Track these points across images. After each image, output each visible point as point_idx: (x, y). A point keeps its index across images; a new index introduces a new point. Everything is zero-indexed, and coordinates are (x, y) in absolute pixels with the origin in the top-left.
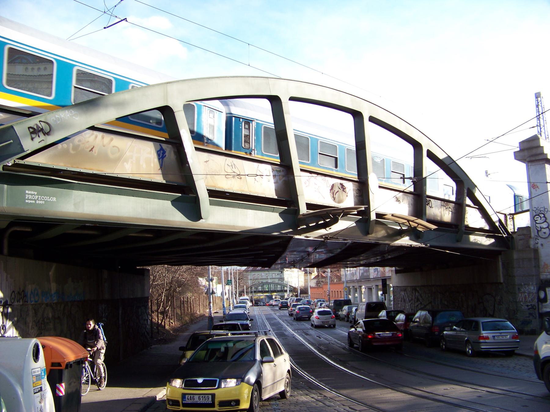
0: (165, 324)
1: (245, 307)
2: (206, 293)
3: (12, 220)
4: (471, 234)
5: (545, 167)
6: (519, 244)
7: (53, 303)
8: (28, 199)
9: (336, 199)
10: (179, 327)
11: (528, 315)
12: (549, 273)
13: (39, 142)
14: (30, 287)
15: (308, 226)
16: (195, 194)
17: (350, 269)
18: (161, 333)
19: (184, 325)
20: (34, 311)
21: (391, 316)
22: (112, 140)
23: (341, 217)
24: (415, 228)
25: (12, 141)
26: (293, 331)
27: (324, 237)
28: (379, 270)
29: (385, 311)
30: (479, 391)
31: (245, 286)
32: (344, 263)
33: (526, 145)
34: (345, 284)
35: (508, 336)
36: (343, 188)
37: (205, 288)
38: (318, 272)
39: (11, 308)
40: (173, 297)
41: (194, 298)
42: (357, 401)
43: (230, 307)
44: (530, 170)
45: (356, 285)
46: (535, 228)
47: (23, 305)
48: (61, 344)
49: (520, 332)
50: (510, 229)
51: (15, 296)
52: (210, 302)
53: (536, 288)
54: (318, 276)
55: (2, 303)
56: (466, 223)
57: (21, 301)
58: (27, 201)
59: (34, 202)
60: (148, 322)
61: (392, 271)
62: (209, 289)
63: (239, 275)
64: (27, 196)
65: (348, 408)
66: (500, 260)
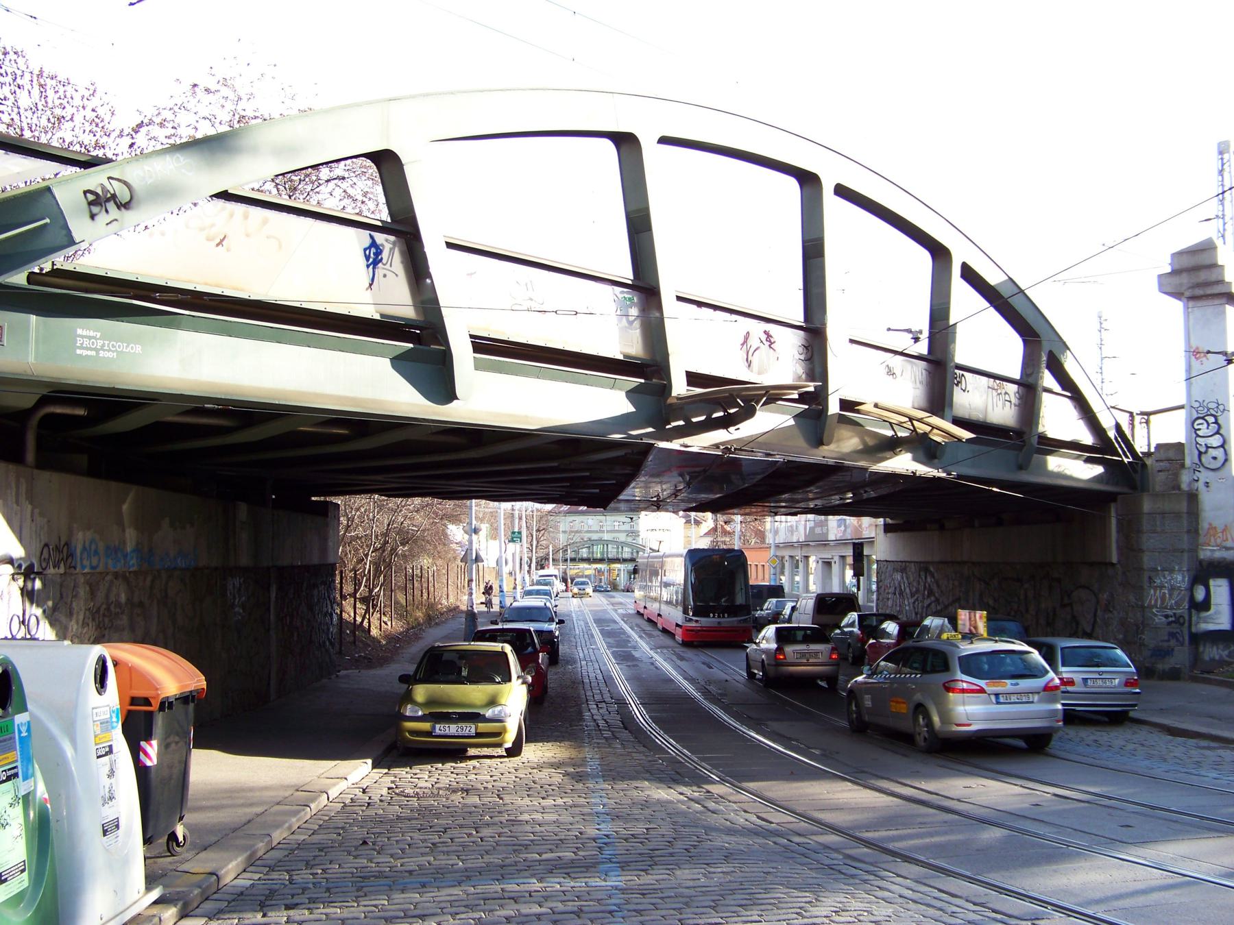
0: (369, 626)
1: (547, 593)
2: (464, 559)
3: (45, 392)
4: (1050, 453)
5: (1224, 312)
6: (1159, 481)
7: (130, 572)
8: (82, 348)
9: (754, 364)
10: (401, 633)
11: (1166, 638)
12: (1218, 546)
13: (107, 224)
14: (80, 535)
15: (688, 421)
16: (441, 345)
17: (786, 519)
18: (361, 645)
19: (413, 628)
20: (88, 588)
21: (870, 626)
22: (265, 222)
23: (763, 405)
24: (925, 434)
25: (48, 220)
26: (651, 649)
27: (722, 447)
28: (848, 522)
29: (855, 614)
30: (1038, 792)
31: (551, 546)
32: (772, 505)
33: (1187, 262)
34: (772, 551)
35: (1117, 681)
36: (770, 341)
37: (461, 547)
38: (716, 521)
39: (41, 579)
40: (389, 566)
41: (435, 568)
42: (777, 806)
43: (515, 593)
44: (1191, 317)
45: (798, 554)
46: (1194, 445)
47: (65, 573)
48: (141, 656)
49: (1146, 672)
50: (1140, 446)
51: (50, 554)
52: (472, 580)
53: (1187, 579)
54: (715, 529)
55: (23, 568)
56: (1041, 429)
57: (62, 565)
58: (79, 352)
59: (93, 353)
60: (332, 619)
61: (876, 526)
62: (468, 551)
63: (539, 521)
64: (79, 342)
65: (754, 818)
66: (1113, 514)
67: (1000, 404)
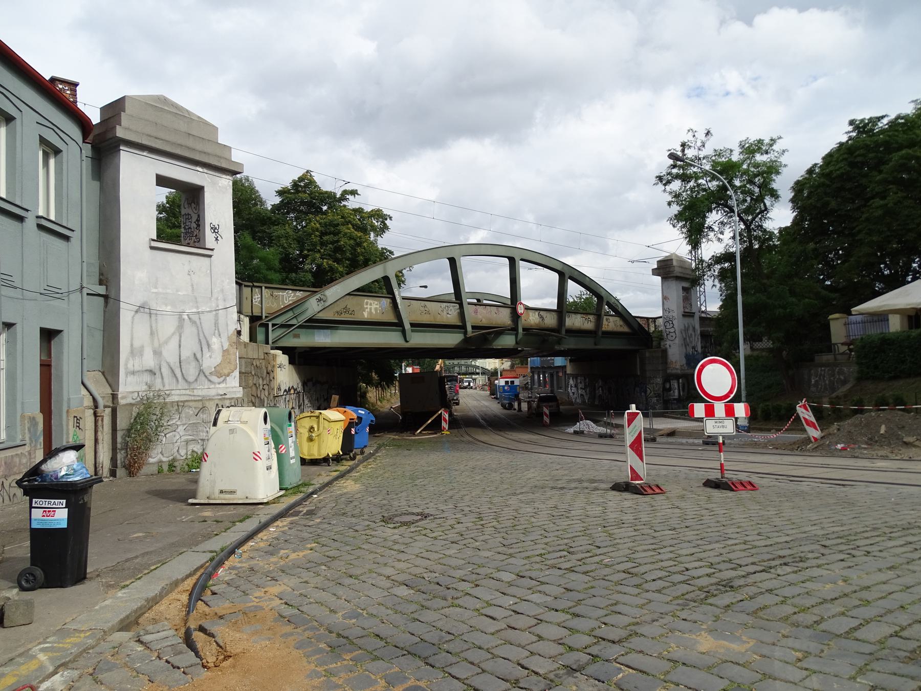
67: (586, 322)
